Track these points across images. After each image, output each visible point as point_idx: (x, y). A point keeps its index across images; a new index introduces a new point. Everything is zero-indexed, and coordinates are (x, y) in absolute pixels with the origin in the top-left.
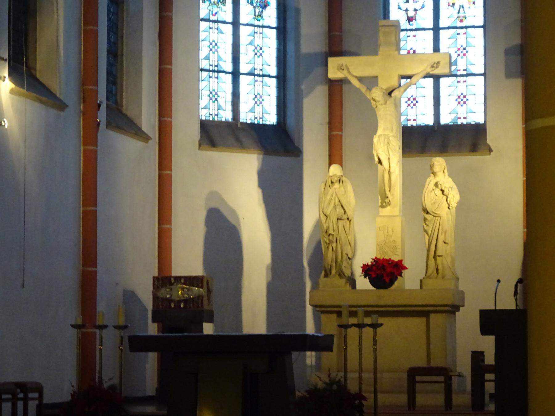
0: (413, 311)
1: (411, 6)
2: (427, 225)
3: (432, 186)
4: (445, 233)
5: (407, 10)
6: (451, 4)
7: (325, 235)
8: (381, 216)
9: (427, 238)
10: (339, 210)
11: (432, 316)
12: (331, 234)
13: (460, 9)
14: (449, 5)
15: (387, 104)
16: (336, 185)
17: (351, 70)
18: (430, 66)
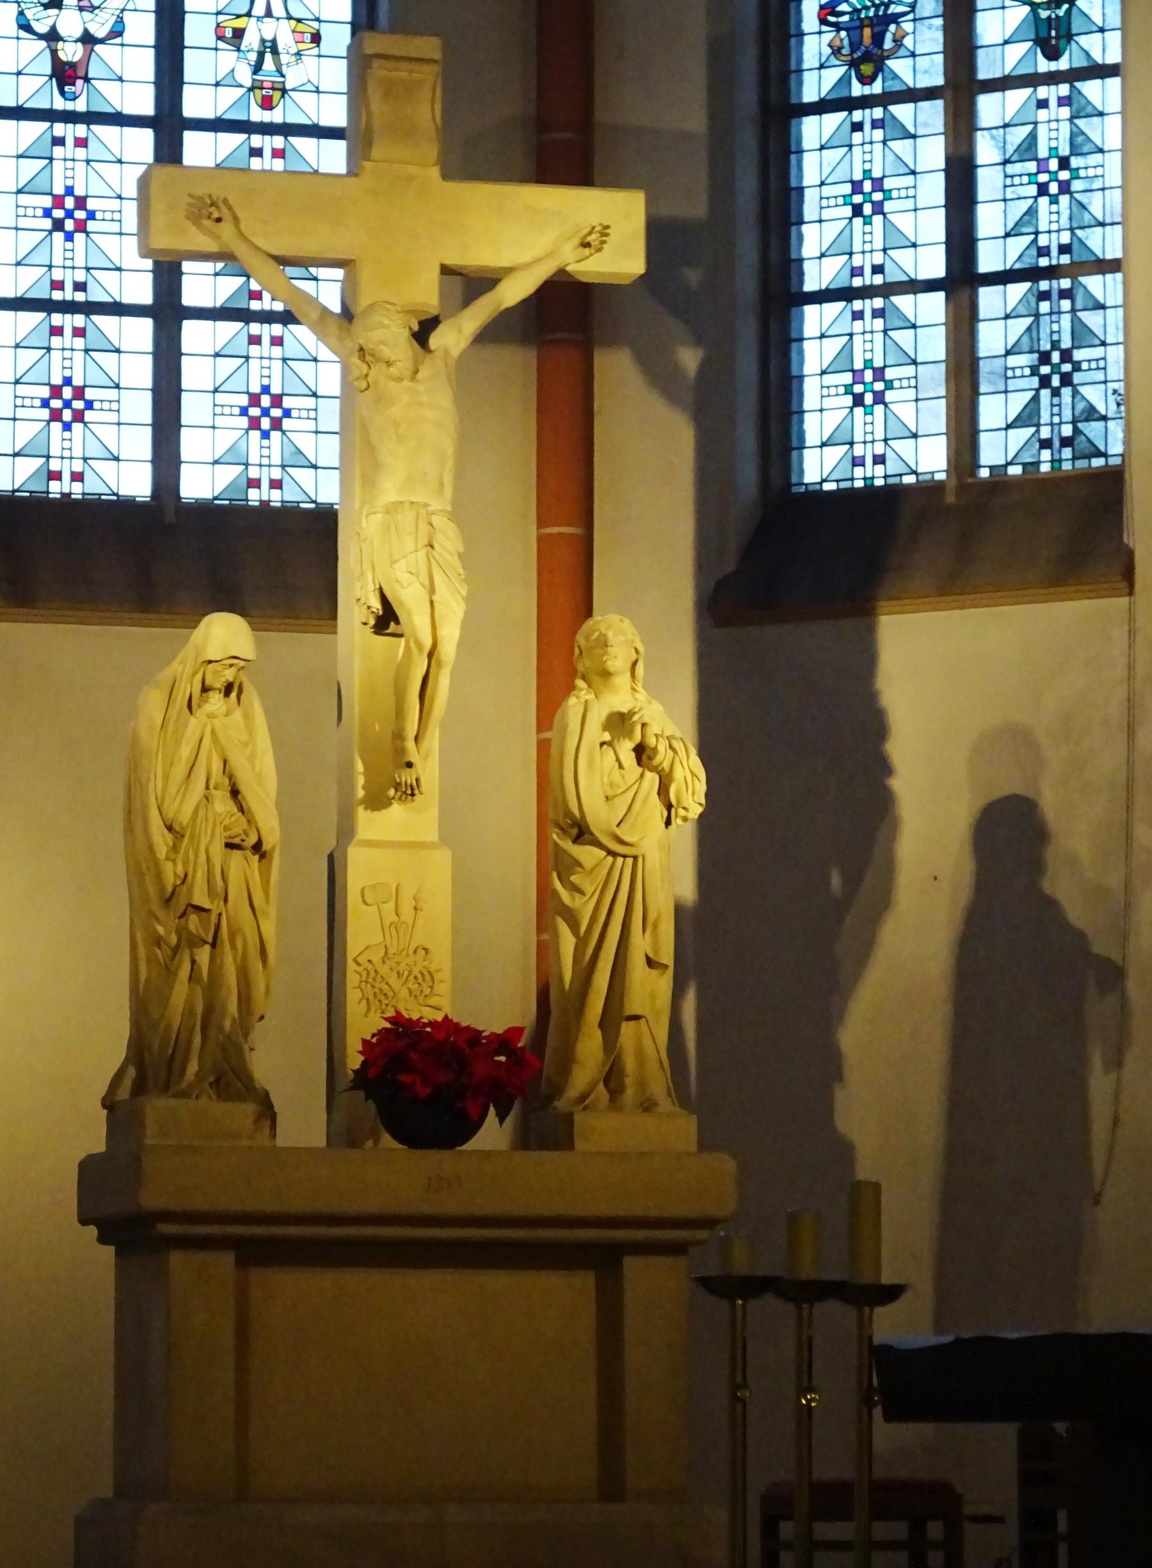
0: (346, 1242)
1: (70, 22)
2: (577, 890)
3: (595, 732)
4: (655, 926)
5: (53, 36)
6: (229, 34)
7: (160, 913)
8: (369, 843)
9: (568, 943)
10: (222, 805)
11: (631, 1264)
12: (199, 909)
13: (261, 56)
14: (220, 38)
15: (420, 376)
16: (216, 702)
17: (242, 226)
18: (576, 241)
